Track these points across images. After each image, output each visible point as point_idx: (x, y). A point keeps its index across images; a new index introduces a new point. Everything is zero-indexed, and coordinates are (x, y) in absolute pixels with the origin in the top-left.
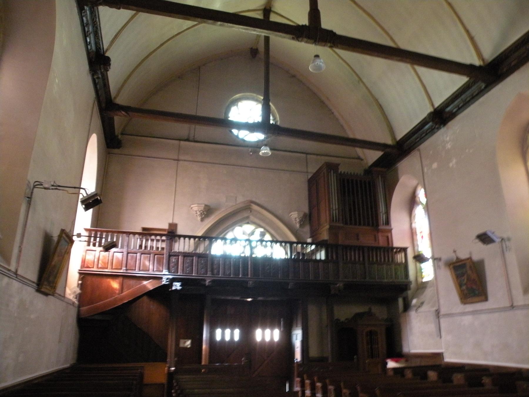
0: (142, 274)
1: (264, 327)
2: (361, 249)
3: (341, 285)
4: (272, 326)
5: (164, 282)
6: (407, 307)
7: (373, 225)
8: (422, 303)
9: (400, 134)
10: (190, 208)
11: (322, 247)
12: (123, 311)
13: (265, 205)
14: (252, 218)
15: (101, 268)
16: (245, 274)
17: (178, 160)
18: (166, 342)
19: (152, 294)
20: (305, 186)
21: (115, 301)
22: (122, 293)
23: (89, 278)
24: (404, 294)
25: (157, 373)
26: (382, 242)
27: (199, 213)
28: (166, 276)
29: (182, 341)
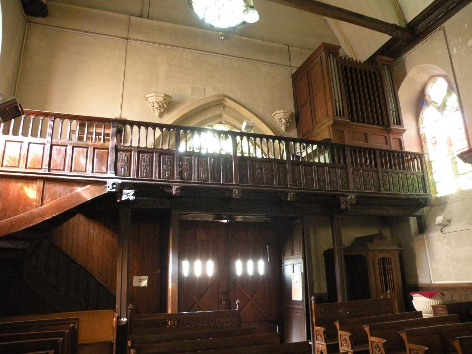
0: (74, 175)
1: (245, 258)
2: (372, 152)
3: (354, 197)
4: (256, 256)
6: (423, 228)
7: (383, 125)
8: (449, 221)
9: (411, 16)
10: (145, 100)
11: (326, 148)
13: (242, 101)
15: (7, 166)
16: (228, 178)
19: (89, 209)
20: (289, 83)
21: (32, 217)
22: (41, 205)
24: (419, 213)
25: (100, 327)
26: (394, 146)
27: (156, 106)
29: (136, 279)
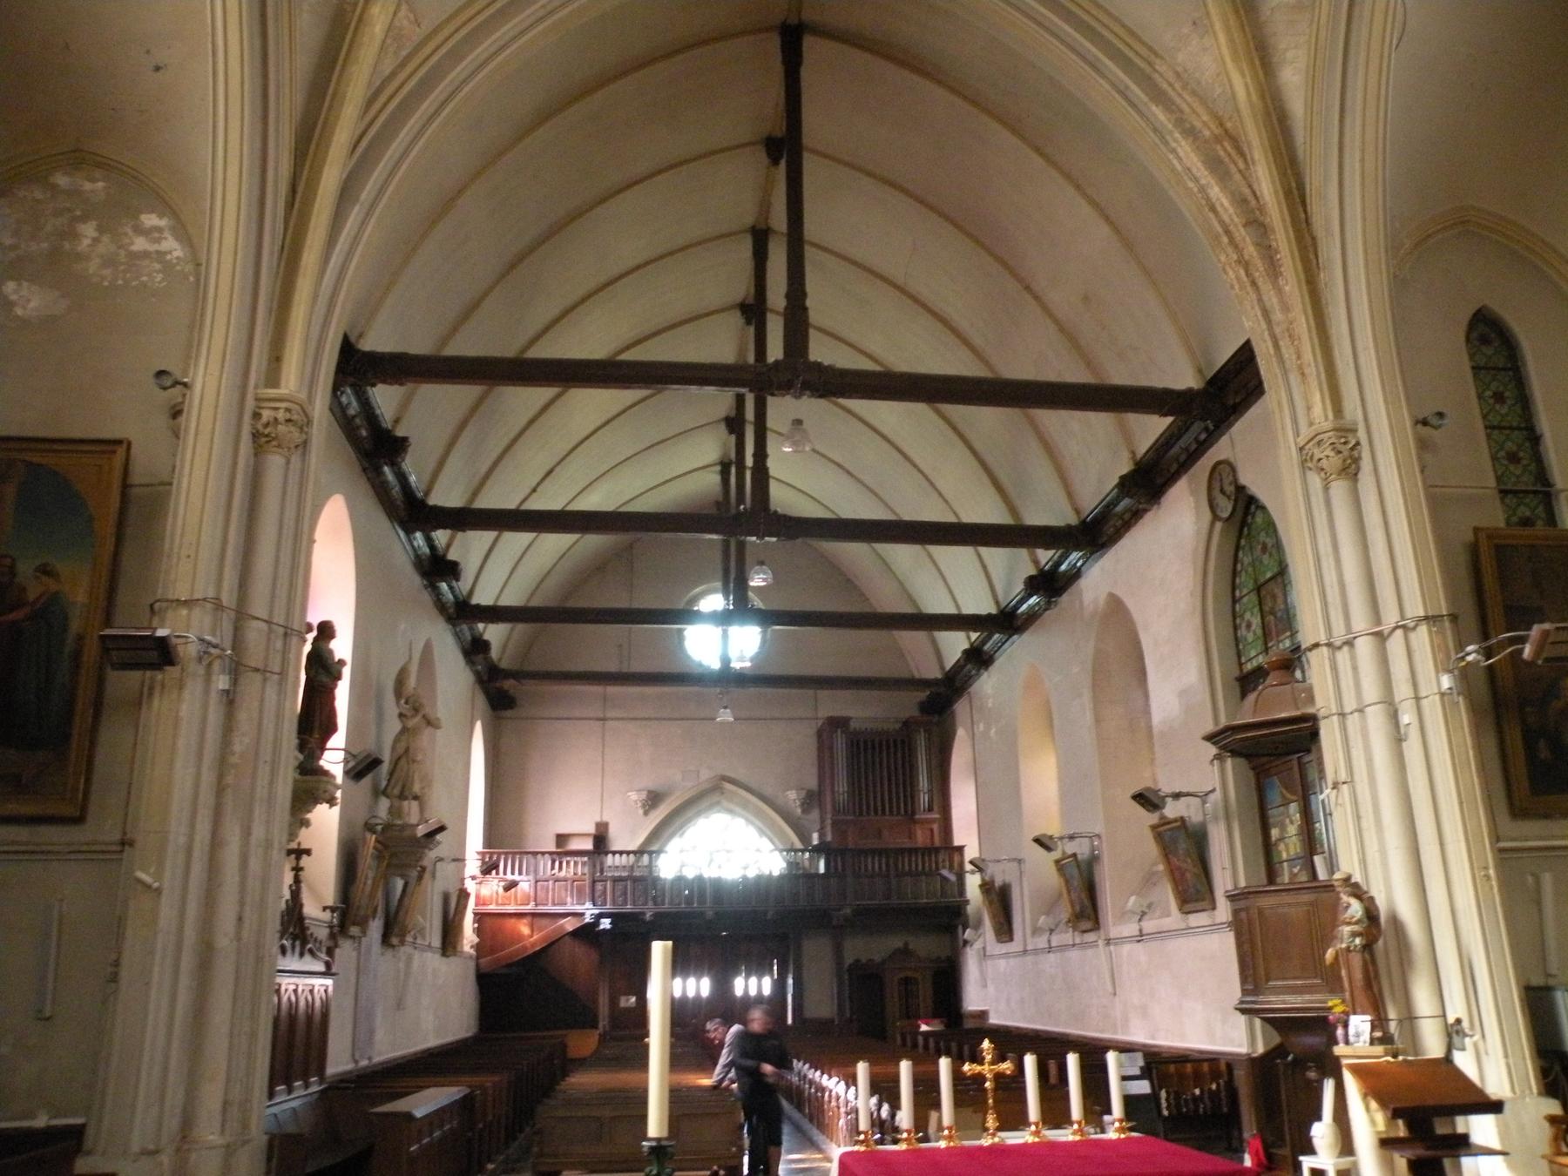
5: (588, 919)
12: (536, 964)
14: (725, 803)
17: (604, 719)
18: (595, 1001)
20: (812, 744)
23: (488, 920)
28: (589, 911)
